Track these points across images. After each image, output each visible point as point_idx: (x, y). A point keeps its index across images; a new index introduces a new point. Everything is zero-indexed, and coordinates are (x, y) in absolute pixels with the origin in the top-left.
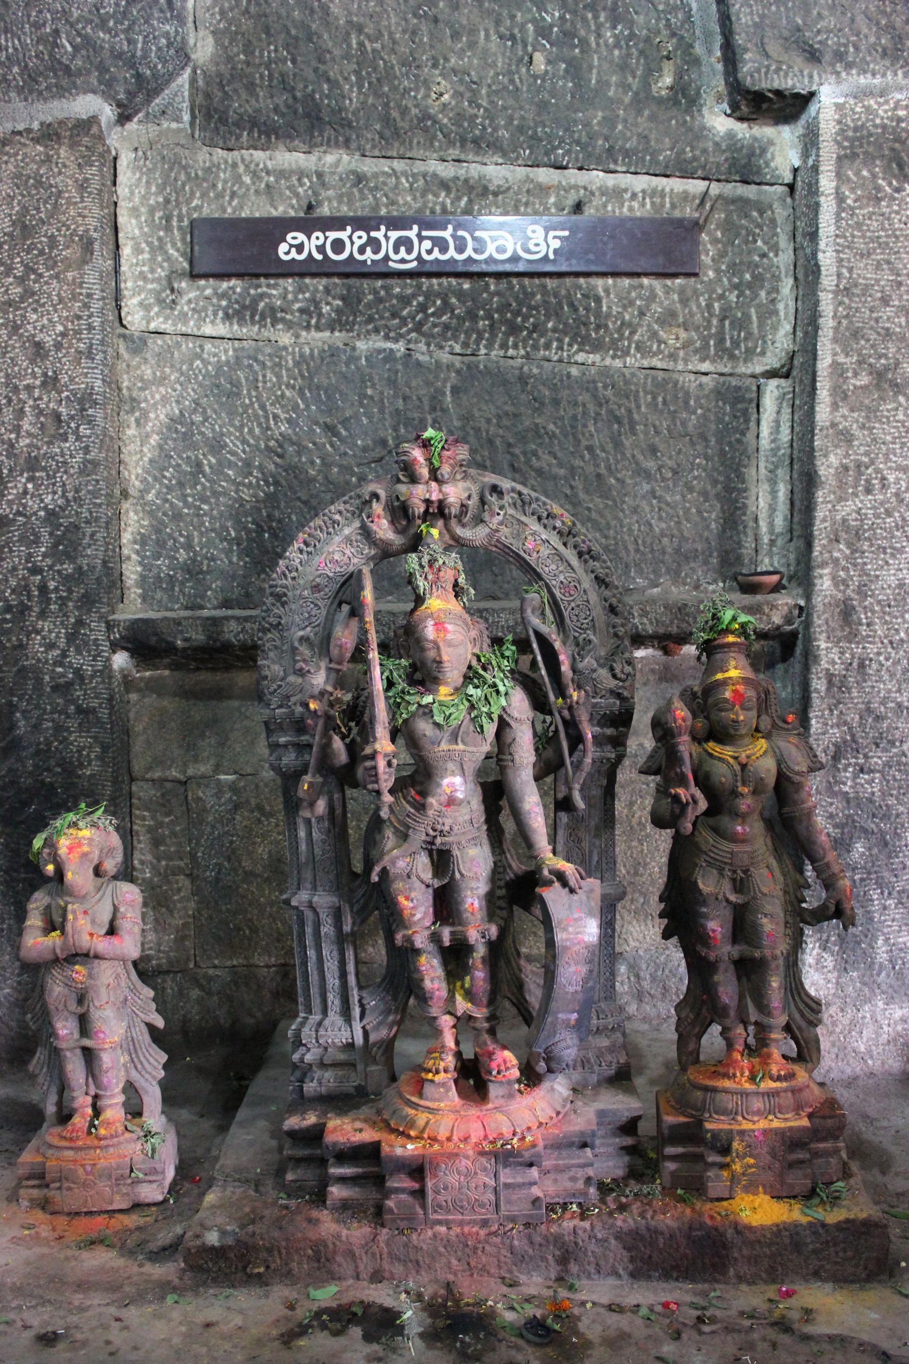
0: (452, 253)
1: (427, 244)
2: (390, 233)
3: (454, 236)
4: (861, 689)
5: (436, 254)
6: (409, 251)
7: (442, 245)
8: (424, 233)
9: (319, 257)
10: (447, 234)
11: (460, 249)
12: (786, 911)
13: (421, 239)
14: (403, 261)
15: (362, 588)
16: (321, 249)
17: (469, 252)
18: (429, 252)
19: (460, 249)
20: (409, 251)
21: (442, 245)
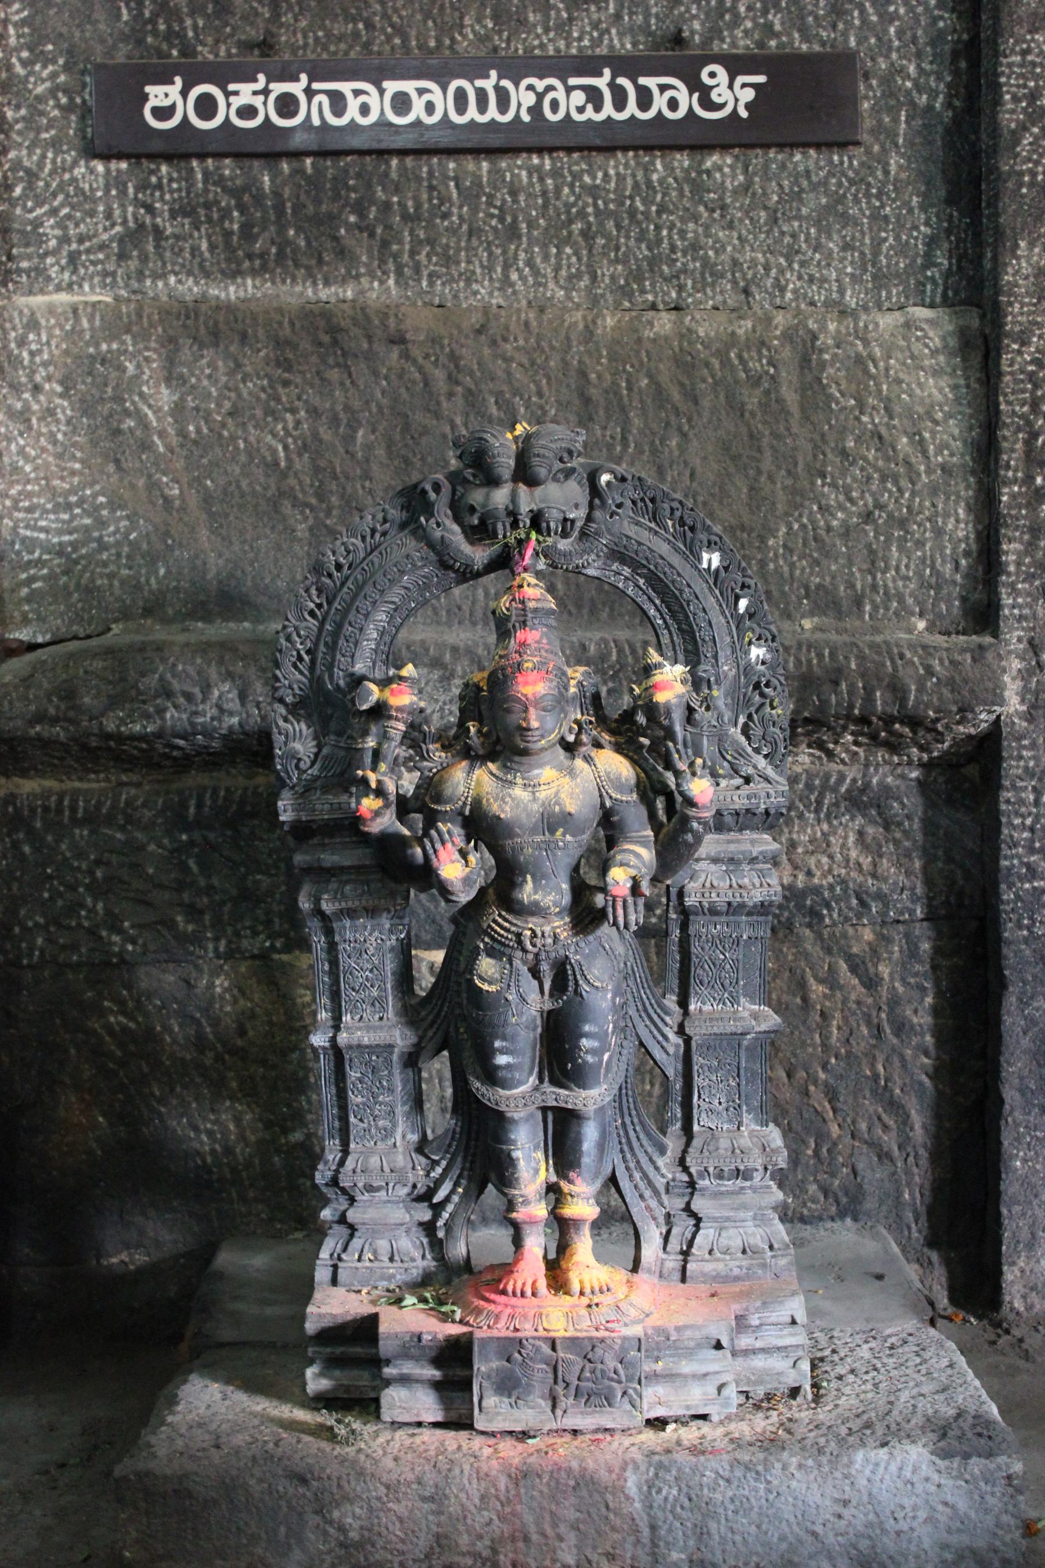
2: (272, 86)
5: (590, 113)
10: (601, 83)
11: (620, 104)
13: (310, 93)
17: (632, 108)
18: (581, 110)
19: (620, 104)
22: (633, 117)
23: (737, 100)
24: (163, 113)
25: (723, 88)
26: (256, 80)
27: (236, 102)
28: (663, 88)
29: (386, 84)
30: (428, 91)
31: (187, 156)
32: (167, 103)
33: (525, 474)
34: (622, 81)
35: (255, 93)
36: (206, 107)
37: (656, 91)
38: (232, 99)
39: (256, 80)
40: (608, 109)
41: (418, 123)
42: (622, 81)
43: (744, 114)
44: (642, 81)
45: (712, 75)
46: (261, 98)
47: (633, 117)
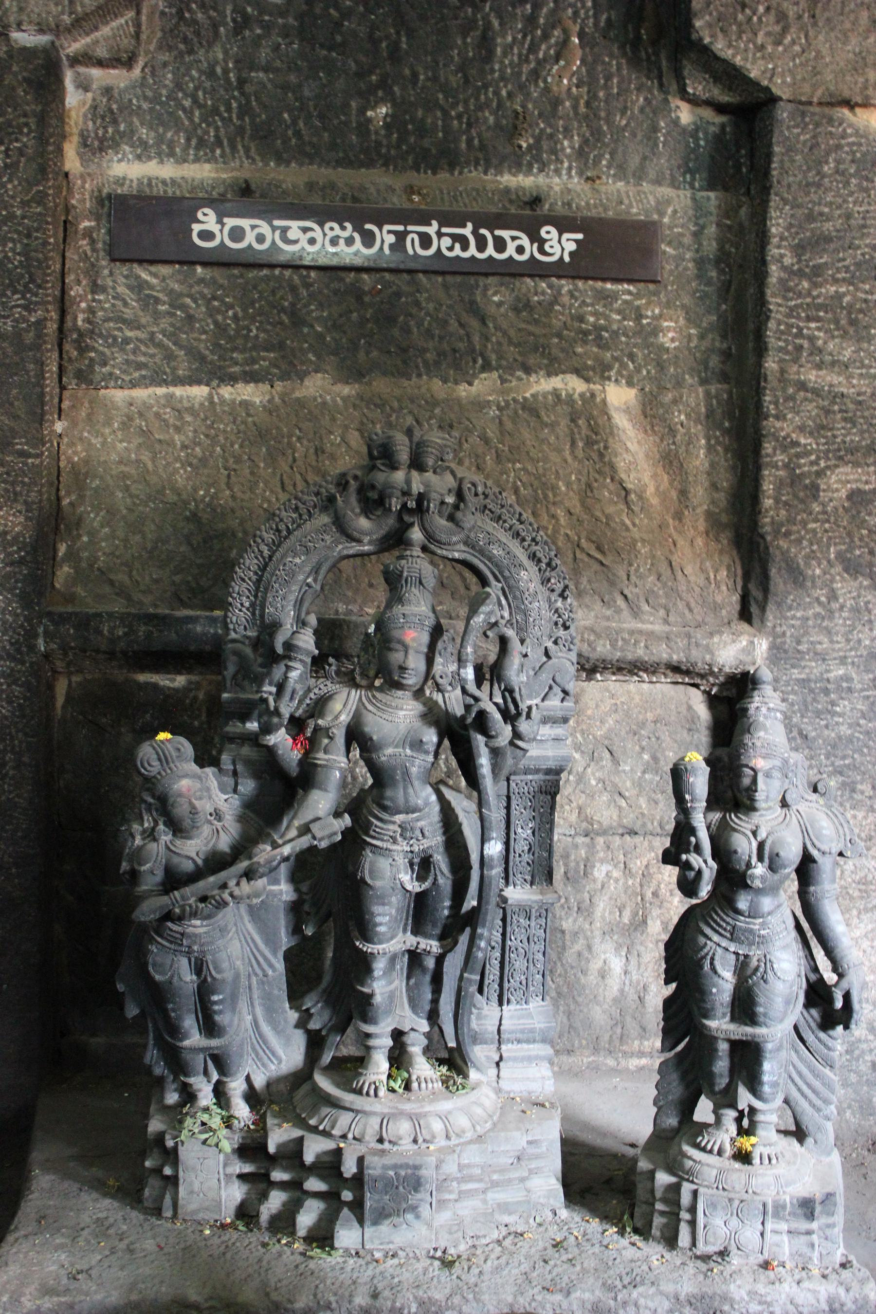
0: (472, 251)
1: (446, 242)
3: (475, 232)
5: (457, 251)
7: (464, 242)
12: (172, 1156)
13: (440, 235)
15: (155, 686)
17: (490, 251)
19: (481, 245)
21: (464, 242)
22: (250, 246)
24: (207, 235)
25: (555, 242)
28: (253, 227)
29: (226, 220)
30: (311, 229)
31: (194, 263)
33: (417, 464)
34: (483, 231)
40: (472, 251)
42: (483, 231)
43: (567, 259)
44: (498, 232)
47: (250, 246)
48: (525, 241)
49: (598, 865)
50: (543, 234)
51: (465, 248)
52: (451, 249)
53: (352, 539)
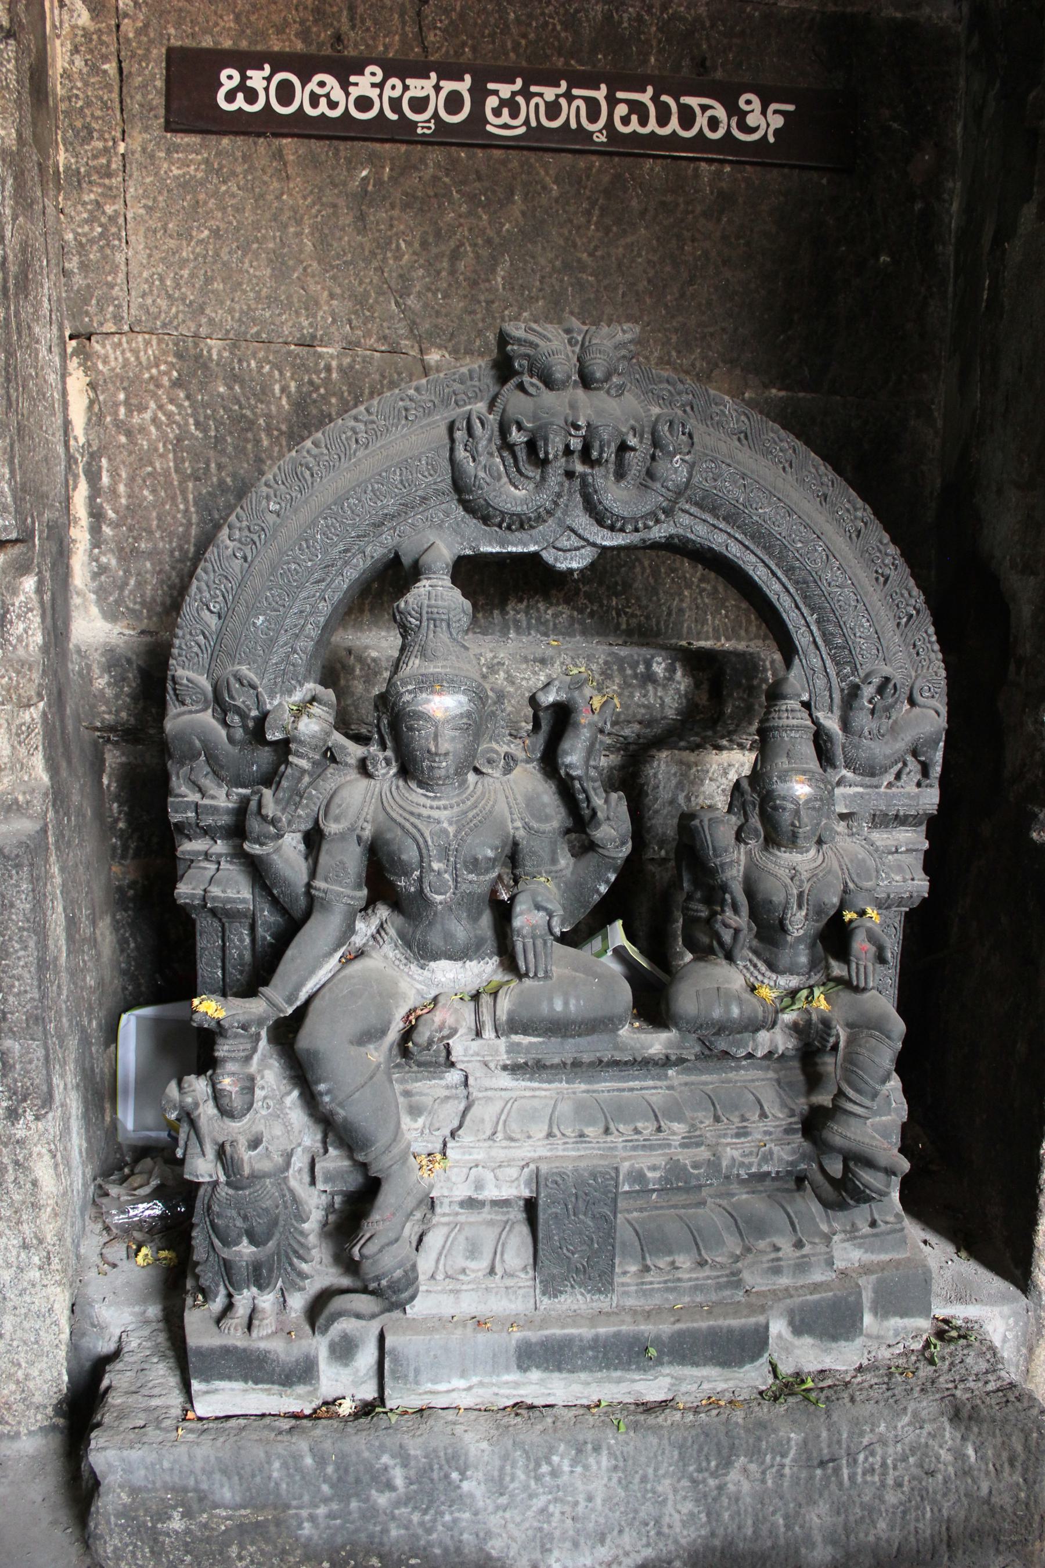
0: (652, 125)
2: (442, 83)
3: (655, 99)
4: (780, 866)
5: (634, 125)
6: (514, 115)
8: (620, 95)
9: (393, 117)
10: (645, 97)
14: (505, 126)
16: (395, 104)
17: (674, 124)
19: (663, 121)
20: (514, 115)
21: (637, 108)
23: (768, 125)
26: (559, 86)
27: (355, 92)
28: (704, 108)
30: (711, 107)
32: (421, 94)
34: (665, 98)
35: (373, 85)
36: (285, 93)
37: (698, 110)
38: (351, 89)
39: (559, 86)
40: (652, 125)
41: (415, 124)
42: (665, 98)
45: (748, 102)
46: (377, 91)
48: (720, 112)
49: (1030, 1386)
50: (741, 103)
51: (643, 122)
52: (626, 121)
53: (183, 704)
